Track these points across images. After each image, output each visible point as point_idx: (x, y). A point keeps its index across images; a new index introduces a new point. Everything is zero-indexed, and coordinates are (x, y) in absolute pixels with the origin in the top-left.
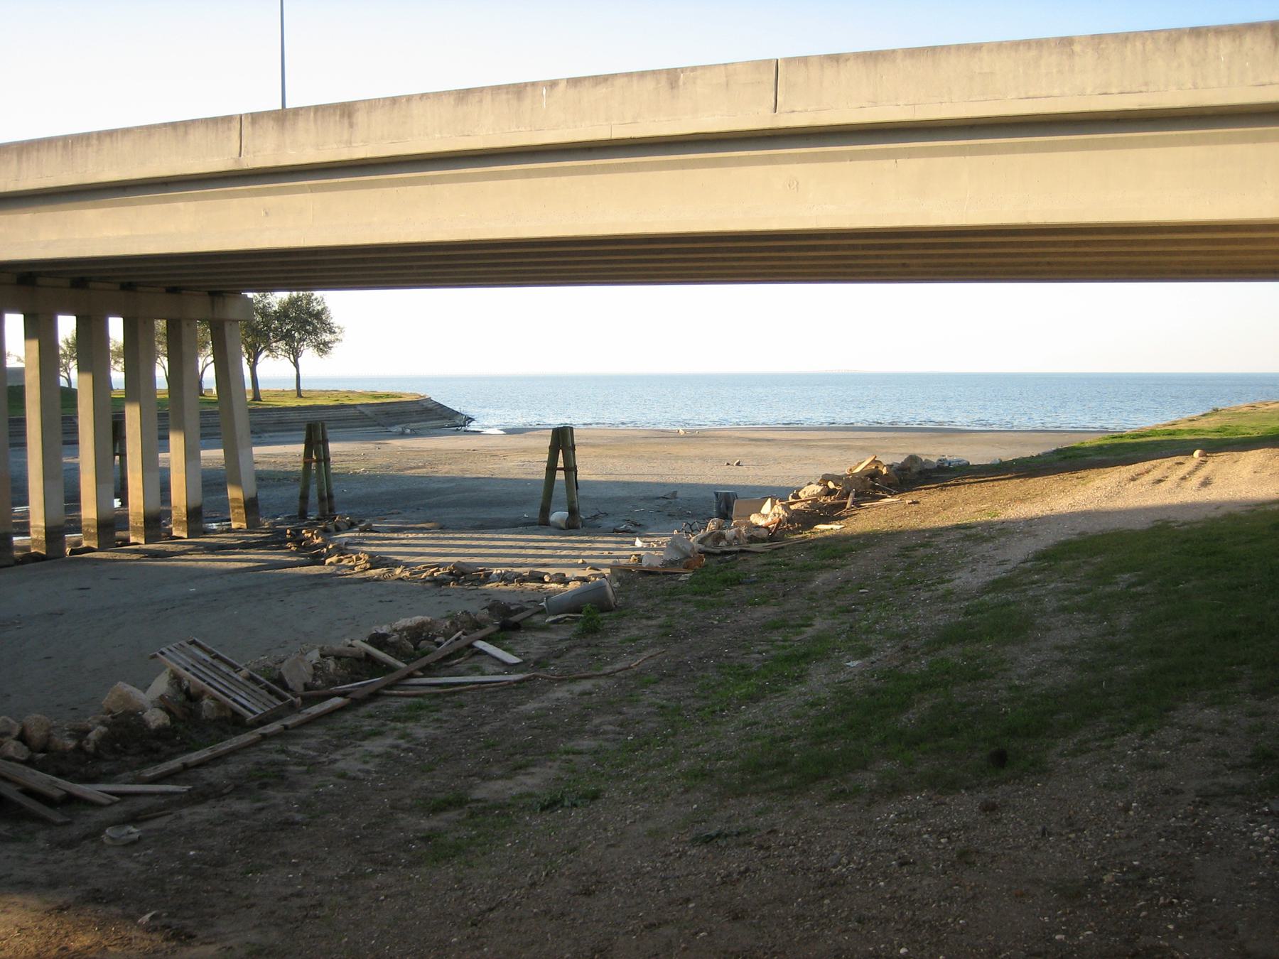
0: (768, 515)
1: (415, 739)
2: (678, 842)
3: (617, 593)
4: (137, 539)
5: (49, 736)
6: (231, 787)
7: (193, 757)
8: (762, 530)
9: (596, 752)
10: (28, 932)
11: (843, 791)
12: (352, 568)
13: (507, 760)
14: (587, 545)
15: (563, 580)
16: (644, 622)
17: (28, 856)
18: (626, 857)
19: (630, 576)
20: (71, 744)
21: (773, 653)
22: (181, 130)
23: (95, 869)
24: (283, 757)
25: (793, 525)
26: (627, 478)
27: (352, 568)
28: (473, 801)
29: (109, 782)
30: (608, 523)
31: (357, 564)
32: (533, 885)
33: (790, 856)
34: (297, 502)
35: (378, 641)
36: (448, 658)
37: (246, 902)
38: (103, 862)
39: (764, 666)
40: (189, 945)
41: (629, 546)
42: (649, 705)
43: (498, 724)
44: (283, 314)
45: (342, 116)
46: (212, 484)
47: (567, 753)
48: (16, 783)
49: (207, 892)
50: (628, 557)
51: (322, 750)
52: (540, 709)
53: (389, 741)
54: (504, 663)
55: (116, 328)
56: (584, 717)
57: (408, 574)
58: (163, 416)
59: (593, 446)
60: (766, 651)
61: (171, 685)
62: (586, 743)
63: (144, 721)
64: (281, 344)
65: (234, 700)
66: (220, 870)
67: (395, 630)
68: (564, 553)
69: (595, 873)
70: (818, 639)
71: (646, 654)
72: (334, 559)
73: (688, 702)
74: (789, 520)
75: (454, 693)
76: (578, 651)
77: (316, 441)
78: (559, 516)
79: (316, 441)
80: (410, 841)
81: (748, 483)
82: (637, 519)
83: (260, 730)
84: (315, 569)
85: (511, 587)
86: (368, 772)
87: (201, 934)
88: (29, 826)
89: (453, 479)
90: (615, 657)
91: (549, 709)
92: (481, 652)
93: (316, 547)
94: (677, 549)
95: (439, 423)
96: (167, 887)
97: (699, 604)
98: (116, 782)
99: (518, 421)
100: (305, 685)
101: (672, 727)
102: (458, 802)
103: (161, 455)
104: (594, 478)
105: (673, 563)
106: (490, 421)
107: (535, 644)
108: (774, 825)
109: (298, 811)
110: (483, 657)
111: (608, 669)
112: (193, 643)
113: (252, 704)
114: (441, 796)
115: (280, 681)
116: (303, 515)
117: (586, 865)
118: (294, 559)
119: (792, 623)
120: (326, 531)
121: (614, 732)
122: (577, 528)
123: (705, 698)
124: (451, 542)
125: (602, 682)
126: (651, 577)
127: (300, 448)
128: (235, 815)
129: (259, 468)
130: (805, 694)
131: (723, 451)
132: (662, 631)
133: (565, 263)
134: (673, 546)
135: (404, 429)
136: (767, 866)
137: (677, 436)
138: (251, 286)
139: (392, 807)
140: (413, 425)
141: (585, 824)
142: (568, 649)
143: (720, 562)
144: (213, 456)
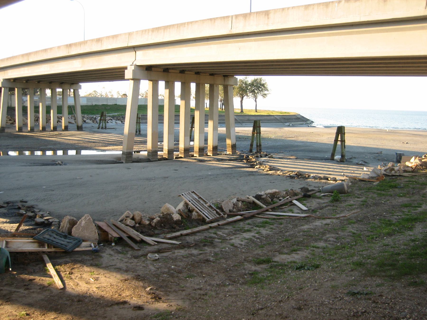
0: (413, 162)
1: (262, 234)
2: (341, 293)
3: (348, 187)
4: (196, 155)
5: (141, 219)
6: (194, 244)
7: (185, 232)
8: (409, 168)
9: (324, 248)
10: (113, 286)
11: (416, 282)
12: (263, 170)
13: (291, 247)
14: (346, 168)
15: (335, 180)
16: (356, 199)
17: (123, 259)
18: (320, 296)
19: (355, 181)
20: (147, 222)
21: (403, 216)
22: (213, 21)
23: (141, 267)
24: (214, 235)
25: (422, 167)
26: (365, 146)
27: (263, 170)
28: (273, 261)
29: (156, 237)
30: (355, 161)
31: (265, 169)
32: (280, 302)
33: (385, 309)
34: (249, 147)
35: (258, 197)
36: (282, 205)
37: (182, 289)
38: (145, 265)
39: (398, 222)
40: (158, 302)
41: (361, 170)
42: (349, 232)
43: (292, 232)
44: (252, 84)
45: (265, 15)
46: (222, 139)
47: (313, 247)
48: (127, 234)
49: (172, 282)
50: (360, 174)
51: (228, 235)
52: (309, 228)
53: (253, 234)
54: (301, 209)
55: (193, 86)
56: (324, 234)
57: (281, 173)
58: (206, 115)
59: (354, 133)
60: (400, 216)
61: (184, 206)
62: (322, 244)
63: (172, 217)
64: (251, 94)
65: (203, 214)
66: (179, 275)
67: (266, 194)
68: (337, 170)
69: (306, 300)
70: (422, 213)
71: (353, 211)
72: (258, 166)
73: (365, 232)
74: (421, 165)
75: (280, 219)
76: (329, 207)
77: (256, 126)
78: (338, 157)
79: (256, 126)
80: (245, 274)
81: (410, 150)
82: (366, 160)
83: (210, 225)
84: (251, 169)
85: (316, 181)
86: (241, 245)
87: (163, 298)
88: (127, 249)
89: (303, 142)
90: (342, 211)
91: (312, 229)
92: (294, 205)
93: (253, 162)
94: (375, 173)
95: (302, 123)
96: (160, 278)
97: (378, 194)
98: (159, 237)
99: (328, 124)
100: (230, 210)
101: (355, 242)
102: (267, 261)
103: (205, 128)
104: (353, 145)
105: (372, 178)
106: (320, 122)
107: (314, 203)
108: (382, 292)
109: (212, 257)
110: (295, 206)
111: (338, 216)
112: (193, 192)
113: (209, 215)
114: (262, 258)
115: (221, 209)
116: (251, 151)
117: (303, 296)
118: (245, 165)
119: (413, 205)
120: (257, 157)
121: (333, 241)
122: (344, 162)
123: (371, 232)
124: (299, 164)
125: (334, 221)
126: (364, 182)
127: (251, 129)
128: (192, 255)
129: (237, 134)
130: (411, 235)
131: (402, 138)
132: (362, 203)
133: (343, 67)
134: (373, 171)
135: (289, 124)
136: (374, 311)
137: (385, 132)
138: (236, 73)
139: (245, 260)
140: (293, 123)
141: (310, 278)
142: (325, 207)
143: (390, 179)
144: (222, 130)
